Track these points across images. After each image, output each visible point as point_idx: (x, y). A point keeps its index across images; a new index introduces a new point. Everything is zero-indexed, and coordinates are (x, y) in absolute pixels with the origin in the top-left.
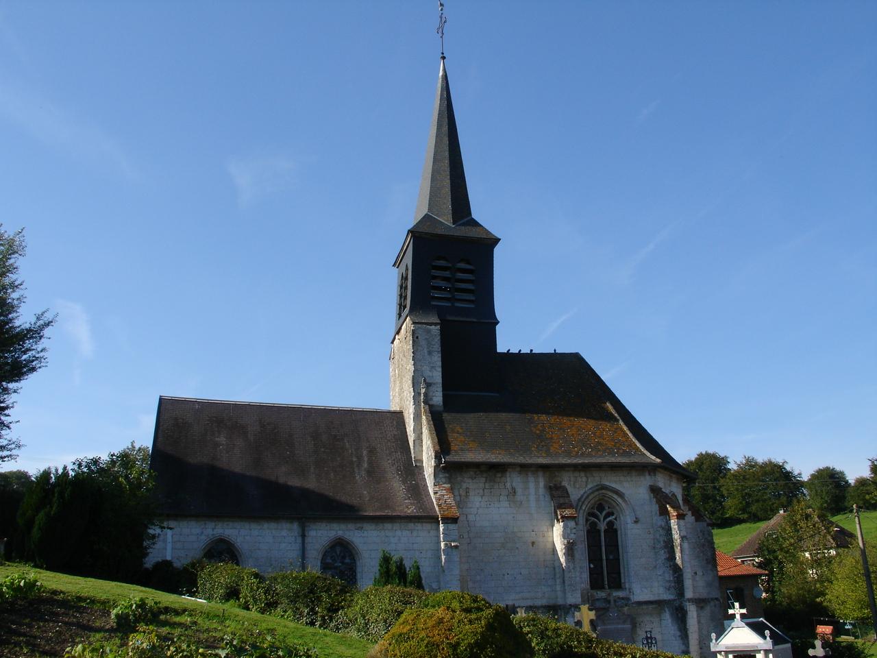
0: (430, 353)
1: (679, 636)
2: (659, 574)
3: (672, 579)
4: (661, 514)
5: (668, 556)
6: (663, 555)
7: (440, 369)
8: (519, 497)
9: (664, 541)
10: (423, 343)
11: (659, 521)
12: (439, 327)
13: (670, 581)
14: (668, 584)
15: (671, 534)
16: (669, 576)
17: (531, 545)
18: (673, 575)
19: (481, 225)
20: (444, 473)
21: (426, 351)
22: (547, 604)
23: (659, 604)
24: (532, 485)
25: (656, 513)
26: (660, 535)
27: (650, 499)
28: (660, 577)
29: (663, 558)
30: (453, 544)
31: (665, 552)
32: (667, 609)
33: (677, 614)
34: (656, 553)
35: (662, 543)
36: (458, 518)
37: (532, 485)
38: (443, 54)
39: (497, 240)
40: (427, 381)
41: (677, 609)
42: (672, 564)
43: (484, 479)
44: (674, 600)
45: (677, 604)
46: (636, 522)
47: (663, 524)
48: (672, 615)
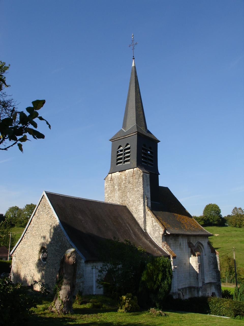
0: (147, 185)
1: (218, 295)
2: (210, 273)
3: (215, 275)
4: (212, 252)
5: (214, 267)
6: (212, 266)
7: (150, 192)
8: (182, 247)
9: (213, 262)
10: (145, 180)
11: (212, 255)
12: (149, 175)
13: (214, 276)
14: (213, 277)
15: (216, 260)
16: (214, 274)
17: (184, 264)
18: (216, 274)
19: (152, 134)
20: (165, 237)
21: (146, 184)
22: (188, 286)
23: (210, 284)
24: (184, 242)
25: (210, 252)
26: (211, 260)
27: (208, 246)
28: (210, 274)
29: (212, 267)
30: (176, 267)
31: (213, 266)
32: (213, 285)
33: (218, 287)
34: (209, 266)
35: (212, 262)
36: (176, 257)
37: (184, 242)
38: (133, 57)
39: (23, 111)
40: (147, 197)
41: (217, 286)
42: (216, 270)
43: (174, 239)
44: (216, 283)
45: (218, 284)
46: (205, 255)
47: (212, 256)
48: (215, 288)
